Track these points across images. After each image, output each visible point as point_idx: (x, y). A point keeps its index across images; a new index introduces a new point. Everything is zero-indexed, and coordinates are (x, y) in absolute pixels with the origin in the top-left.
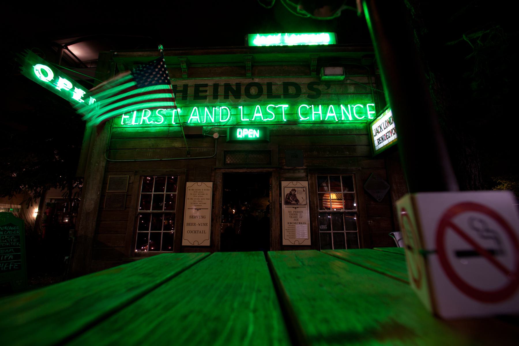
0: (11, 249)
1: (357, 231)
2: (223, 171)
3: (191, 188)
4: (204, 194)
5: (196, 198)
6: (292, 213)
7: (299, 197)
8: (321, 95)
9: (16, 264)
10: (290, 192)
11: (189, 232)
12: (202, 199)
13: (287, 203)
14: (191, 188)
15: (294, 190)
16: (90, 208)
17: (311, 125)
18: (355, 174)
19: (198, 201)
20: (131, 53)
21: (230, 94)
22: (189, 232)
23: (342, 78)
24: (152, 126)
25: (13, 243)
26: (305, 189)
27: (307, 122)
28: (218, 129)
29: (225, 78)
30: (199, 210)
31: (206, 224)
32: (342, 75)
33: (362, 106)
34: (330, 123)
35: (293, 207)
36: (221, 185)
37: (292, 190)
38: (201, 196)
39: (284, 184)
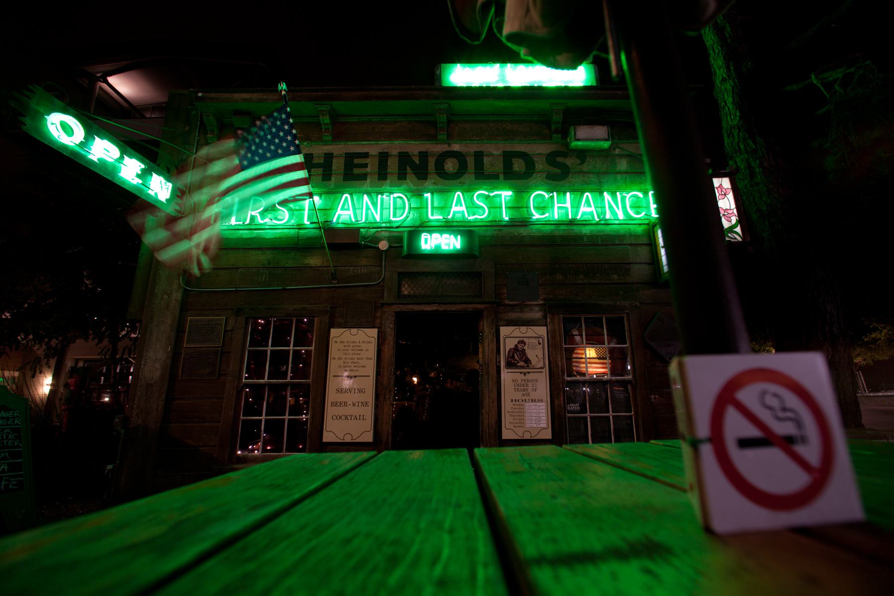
0: (5, 452)
1: (633, 413)
2: (397, 308)
3: (338, 340)
4: (362, 350)
5: (347, 356)
6: (519, 382)
7: (531, 354)
8: (570, 175)
9: (14, 481)
10: (516, 346)
11: (334, 417)
12: (358, 359)
13: (510, 365)
14: (338, 340)
15: (523, 342)
16: (153, 375)
17: (552, 227)
18: (628, 314)
19: (352, 363)
20: (229, 95)
21: (409, 170)
22: (334, 417)
23: (606, 145)
24: (267, 227)
25: (7, 442)
26: (541, 341)
27: (544, 223)
28: (387, 234)
29: (400, 142)
30: (527, 374)
31: (365, 404)
32: (606, 140)
33: (640, 195)
34: (585, 224)
35: (521, 373)
36: (393, 333)
37: (519, 343)
38: (357, 354)
39: (504, 331)
